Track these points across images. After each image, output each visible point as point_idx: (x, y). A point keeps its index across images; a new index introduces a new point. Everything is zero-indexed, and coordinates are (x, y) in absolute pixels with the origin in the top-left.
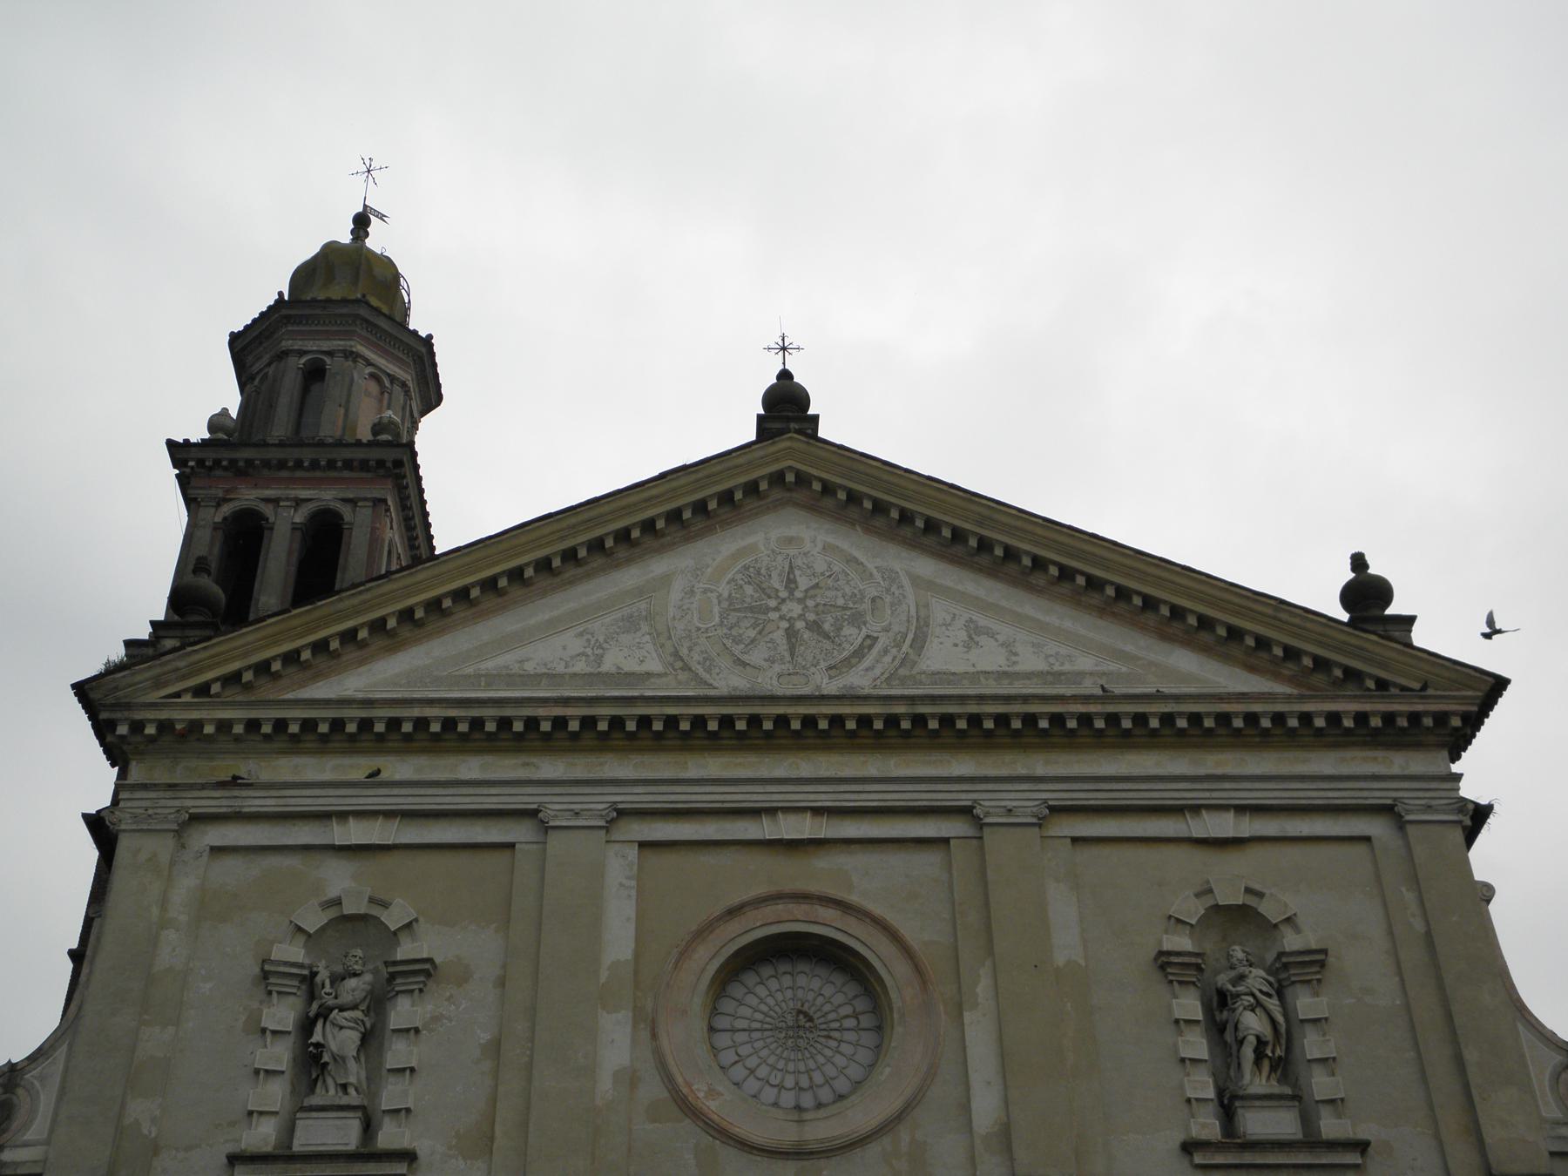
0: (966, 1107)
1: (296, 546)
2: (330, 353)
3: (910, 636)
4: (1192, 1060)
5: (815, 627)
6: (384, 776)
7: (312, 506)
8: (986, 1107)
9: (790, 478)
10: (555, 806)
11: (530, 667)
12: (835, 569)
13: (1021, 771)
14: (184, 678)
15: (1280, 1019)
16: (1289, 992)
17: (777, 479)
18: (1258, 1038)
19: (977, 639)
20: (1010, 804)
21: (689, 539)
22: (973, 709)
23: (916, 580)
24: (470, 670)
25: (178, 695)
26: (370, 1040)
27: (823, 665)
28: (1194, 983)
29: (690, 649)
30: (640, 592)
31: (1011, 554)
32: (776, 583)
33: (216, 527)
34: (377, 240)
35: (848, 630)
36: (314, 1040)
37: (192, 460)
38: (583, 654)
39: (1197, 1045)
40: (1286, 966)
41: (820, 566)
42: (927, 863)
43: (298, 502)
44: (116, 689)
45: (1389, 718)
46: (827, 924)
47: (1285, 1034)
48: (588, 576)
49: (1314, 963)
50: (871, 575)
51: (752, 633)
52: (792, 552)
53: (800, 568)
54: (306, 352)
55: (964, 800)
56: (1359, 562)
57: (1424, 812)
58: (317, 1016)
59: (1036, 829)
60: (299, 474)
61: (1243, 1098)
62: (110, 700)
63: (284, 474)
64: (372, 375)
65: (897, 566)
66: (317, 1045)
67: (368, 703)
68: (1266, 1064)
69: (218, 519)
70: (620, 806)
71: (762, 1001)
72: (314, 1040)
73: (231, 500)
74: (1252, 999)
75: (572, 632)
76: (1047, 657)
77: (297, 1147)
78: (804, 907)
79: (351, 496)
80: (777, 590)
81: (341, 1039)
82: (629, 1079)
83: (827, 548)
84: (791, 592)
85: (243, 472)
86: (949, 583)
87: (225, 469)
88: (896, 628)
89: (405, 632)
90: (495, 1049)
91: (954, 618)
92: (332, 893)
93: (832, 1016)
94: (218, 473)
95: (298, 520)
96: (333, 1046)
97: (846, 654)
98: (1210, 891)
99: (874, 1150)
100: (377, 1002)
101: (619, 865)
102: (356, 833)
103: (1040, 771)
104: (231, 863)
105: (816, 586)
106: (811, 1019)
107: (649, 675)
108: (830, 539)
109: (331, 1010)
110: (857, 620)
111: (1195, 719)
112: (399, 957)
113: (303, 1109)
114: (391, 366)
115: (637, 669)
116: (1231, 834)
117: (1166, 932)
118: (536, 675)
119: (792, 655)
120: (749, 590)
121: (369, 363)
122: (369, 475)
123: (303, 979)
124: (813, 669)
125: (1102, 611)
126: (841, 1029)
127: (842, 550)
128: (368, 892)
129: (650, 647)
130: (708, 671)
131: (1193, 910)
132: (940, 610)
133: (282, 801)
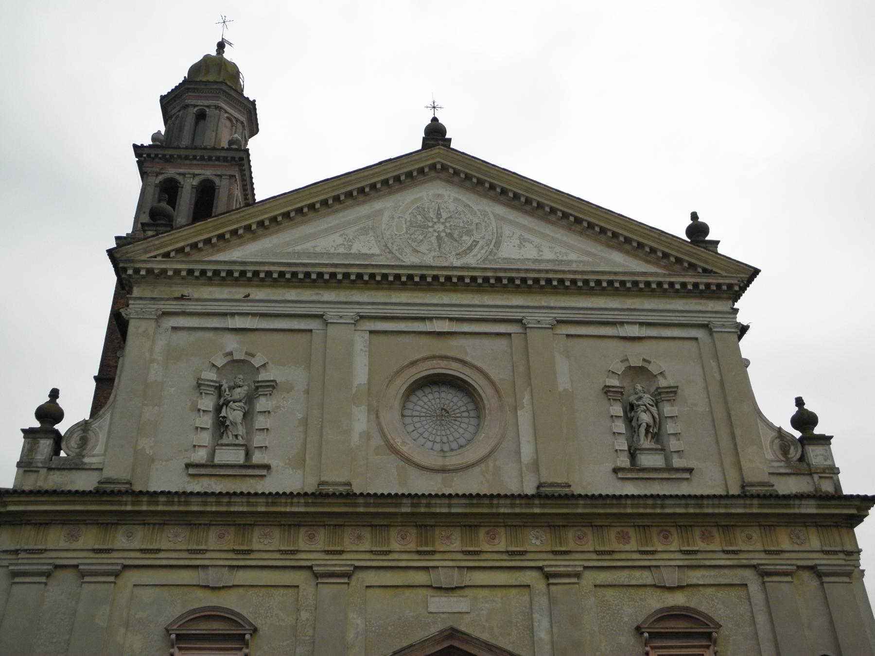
0: (518, 452)
1: (194, 195)
2: (208, 107)
3: (494, 241)
5: (450, 235)
6: (251, 297)
7: (201, 177)
8: (527, 452)
9: (439, 167)
10: (331, 313)
11: (318, 250)
14: (157, 249)
15: (657, 416)
16: (660, 405)
17: (433, 167)
19: (524, 244)
21: (391, 193)
22: (523, 275)
23: (496, 216)
24: (290, 250)
25: (155, 257)
26: (247, 415)
27: (454, 253)
30: (369, 216)
35: (465, 238)
37: (145, 154)
39: (620, 427)
40: (660, 393)
41: (452, 208)
42: (501, 344)
44: (127, 253)
45: (708, 286)
46: (455, 370)
48: (345, 209)
49: (673, 391)
51: (421, 237)
52: (439, 201)
54: (197, 106)
55: (518, 316)
61: (640, 450)
62: (124, 258)
63: (188, 162)
64: (228, 118)
65: (488, 209)
66: (224, 417)
68: (650, 435)
69: (157, 182)
71: (423, 408)
73: (163, 173)
75: (337, 234)
76: (556, 253)
77: (216, 461)
78: (445, 362)
79: (219, 173)
80: (432, 218)
81: (234, 414)
82: (366, 436)
83: (455, 200)
85: (168, 160)
87: (160, 159)
92: (228, 350)
93: (458, 411)
95: (194, 183)
98: (627, 360)
99: (477, 469)
100: (250, 399)
101: (360, 341)
104: (181, 334)
105: (450, 217)
106: (448, 412)
108: (457, 196)
110: (469, 233)
114: (236, 114)
115: (368, 252)
117: (608, 377)
118: (321, 253)
119: (440, 248)
120: (419, 218)
121: (226, 112)
123: (216, 387)
128: (245, 349)
131: (620, 368)
133: (204, 307)
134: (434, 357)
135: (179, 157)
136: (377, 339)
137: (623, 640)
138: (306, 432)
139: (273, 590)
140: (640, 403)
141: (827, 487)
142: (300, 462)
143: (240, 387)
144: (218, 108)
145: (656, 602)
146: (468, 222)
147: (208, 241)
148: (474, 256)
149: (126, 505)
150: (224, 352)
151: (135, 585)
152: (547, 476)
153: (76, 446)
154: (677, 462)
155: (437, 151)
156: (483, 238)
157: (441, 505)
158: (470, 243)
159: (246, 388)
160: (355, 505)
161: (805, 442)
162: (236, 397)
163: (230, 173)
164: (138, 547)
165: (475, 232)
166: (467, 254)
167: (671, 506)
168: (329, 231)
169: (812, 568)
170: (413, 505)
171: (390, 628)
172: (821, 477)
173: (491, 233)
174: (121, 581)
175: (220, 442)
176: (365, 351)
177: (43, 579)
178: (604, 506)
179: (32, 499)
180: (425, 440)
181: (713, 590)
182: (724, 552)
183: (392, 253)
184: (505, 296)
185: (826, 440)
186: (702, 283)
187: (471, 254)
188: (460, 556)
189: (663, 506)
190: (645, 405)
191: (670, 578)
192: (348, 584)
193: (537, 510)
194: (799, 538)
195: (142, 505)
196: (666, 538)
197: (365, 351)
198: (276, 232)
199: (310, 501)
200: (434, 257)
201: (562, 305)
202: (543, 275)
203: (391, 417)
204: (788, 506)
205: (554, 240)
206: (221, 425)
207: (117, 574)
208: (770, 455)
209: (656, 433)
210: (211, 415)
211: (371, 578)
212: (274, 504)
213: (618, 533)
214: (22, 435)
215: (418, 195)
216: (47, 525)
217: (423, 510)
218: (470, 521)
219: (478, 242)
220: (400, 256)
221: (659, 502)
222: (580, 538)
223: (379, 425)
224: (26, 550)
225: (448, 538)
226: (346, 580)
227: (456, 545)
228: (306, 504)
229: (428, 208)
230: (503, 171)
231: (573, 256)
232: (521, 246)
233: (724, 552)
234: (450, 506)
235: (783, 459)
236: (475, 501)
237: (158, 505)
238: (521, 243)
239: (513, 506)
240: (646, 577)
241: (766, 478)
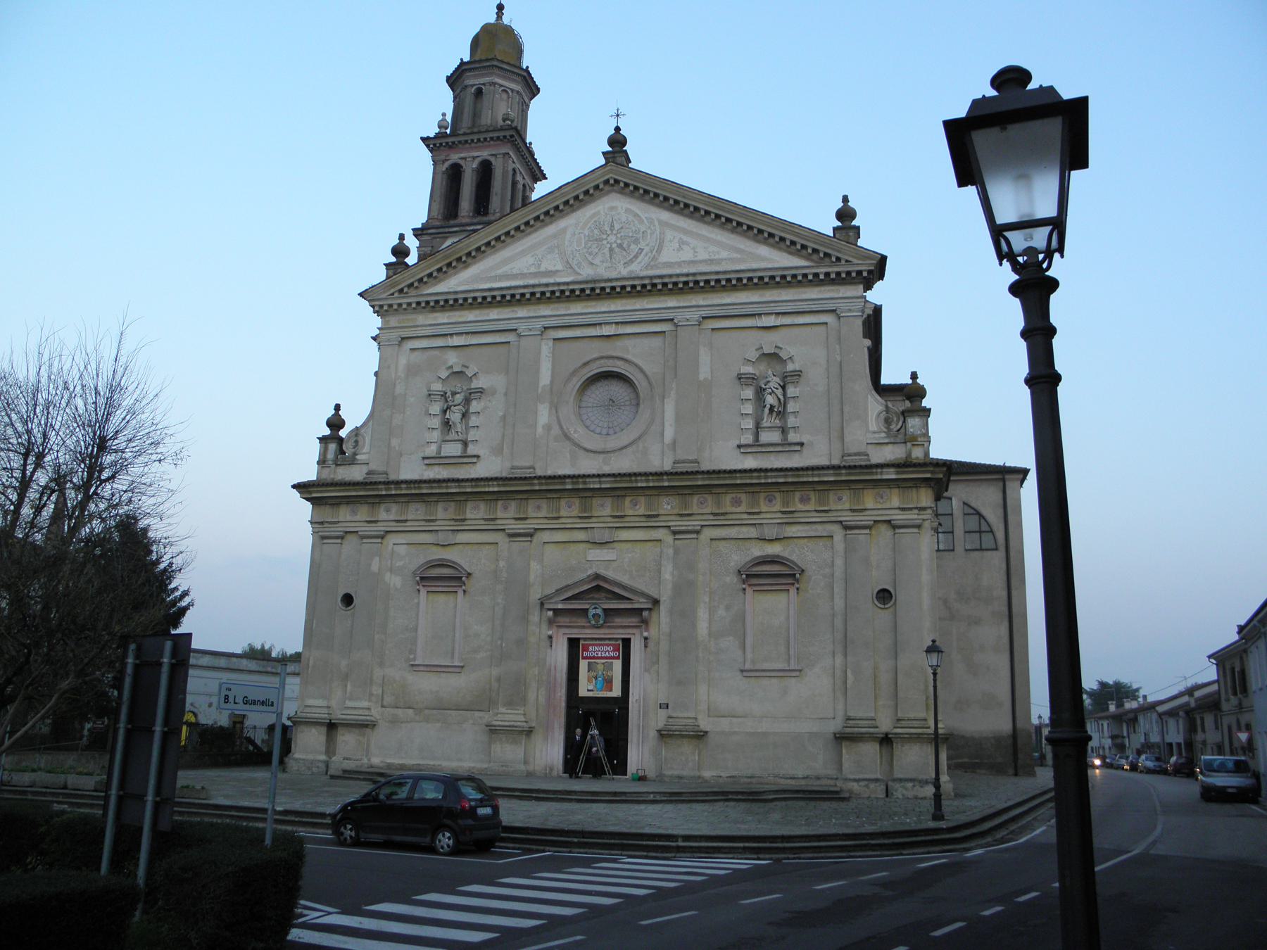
0: (662, 435)
1: (474, 178)
2: (484, 84)
3: (656, 247)
4: (745, 414)
5: (620, 246)
7: (480, 159)
8: (669, 434)
9: (612, 182)
10: (522, 327)
11: (514, 272)
12: (630, 219)
13: (694, 303)
17: (607, 182)
18: (771, 405)
19: (682, 246)
20: (688, 317)
21: (573, 211)
22: (674, 280)
23: (660, 222)
24: (493, 274)
25: (393, 294)
26: (465, 415)
27: (622, 262)
28: (751, 385)
29: (573, 259)
30: (555, 236)
31: (697, 209)
32: (607, 228)
33: (444, 173)
34: (506, 20)
35: (633, 246)
36: (446, 417)
38: (533, 264)
39: (749, 408)
40: (786, 377)
41: (624, 219)
42: (656, 342)
43: (474, 158)
45: (838, 274)
46: (620, 367)
48: (536, 230)
49: (798, 374)
50: (643, 221)
51: (597, 250)
52: (613, 213)
53: (615, 220)
54: (474, 85)
55: (671, 316)
56: (845, 199)
57: (848, 312)
58: (447, 409)
59: (697, 327)
63: (467, 145)
64: (503, 90)
65: (653, 216)
66: (448, 419)
67: (456, 293)
68: (775, 414)
69: (444, 169)
70: (546, 326)
71: (595, 400)
72: (446, 417)
74: (770, 390)
75: (530, 255)
77: (442, 454)
78: (611, 361)
79: (494, 153)
80: (606, 231)
81: (455, 416)
82: (548, 428)
83: (628, 211)
84: (612, 230)
85: (451, 146)
87: (444, 146)
88: (651, 245)
89: (469, 260)
90: (504, 418)
91: (674, 237)
92: (450, 364)
93: (622, 401)
95: (474, 166)
96: (452, 419)
97: (631, 257)
98: (762, 348)
99: (630, 450)
100: (467, 401)
101: (546, 348)
102: (457, 341)
103: (702, 303)
104: (416, 353)
105: (622, 228)
106: (614, 402)
107: (557, 271)
108: (629, 206)
109: (451, 406)
110: (636, 241)
111: (761, 278)
112: (472, 387)
113: (443, 441)
115: (554, 269)
116: (772, 324)
117: (743, 365)
118: (517, 274)
119: (611, 259)
121: (501, 86)
123: (442, 395)
124: (619, 265)
126: (625, 405)
127: (633, 211)
129: (558, 259)
130: (579, 268)
131: (753, 355)
132: (669, 234)
134: (602, 358)
135: (460, 142)
136: (559, 345)
137: (728, 579)
138: (504, 427)
139: (482, 546)
140: (767, 386)
141: (917, 453)
142: (498, 451)
143: (459, 393)
144: (494, 84)
145: (758, 551)
146: (636, 230)
147: (430, 275)
149: (382, 490)
150: (447, 366)
151: (394, 544)
152: (681, 455)
153: (352, 447)
154: (792, 437)
155: (609, 168)
156: (648, 245)
157: (594, 483)
159: (463, 394)
160: (533, 484)
161: (906, 414)
162: (456, 403)
163: (504, 152)
164: (393, 519)
165: (641, 241)
166: (632, 262)
167: (771, 477)
168: (523, 253)
169: (889, 522)
170: (573, 483)
171: (559, 572)
172: (913, 445)
173: (654, 240)
174: (385, 541)
175: (447, 438)
176: (549, 357)
177: (339, 541)
178: (719, 479)
179: (324, 489)
180: (595, 426)
181: (806, 540)
182: (816, 511)
183: (572, 268)
184: (662, 298)
185: (927, 412)
186: (832, 272)
188: (610, 519)
189: (766, 477)
190: (771, 388)
191: (770, 532)
192: (531, 541)
193: (666, 484)
194: (882, 498)
195: (391, 490)
196: (770, 501)
197: (549, 357)
198: (481, 260)
199: (501, 483)
200: (606, 268)
201: (709, 302)
202: (691, 278)
203: (568, 410)
204: (872, 474)
205: (708, 240)
206: (447, 424)
207: (382, 537)
208: (873, 426)
209: (780, 412)
210: (439, 417)
211: (546, 536)
212: (476, 486)
213: (733, 498)
214: (318, 441)
215: (597, 210)
216: (338, 504)
217: (581, 486)
218: (619, 493)
219: (643, 249)
220: (578, 270)
221: (762, 474)
222: (701, 503)
223: (558, 418)
224: (327, 522)
225: (602, 505)
226: (529, 539)
227: (607, 511)
228: (499, 486)
229: (603, 222)
230: (664, 181)
231: (724, 254)
232: (680, 249)
233: (816, 511)
234: (600, 482)
235: (885, 430)
236: (618, 479)
237: (402, 490)
238: (680, 247)
239: (647, 481)
240: (752, 532)
241: (863, 449)
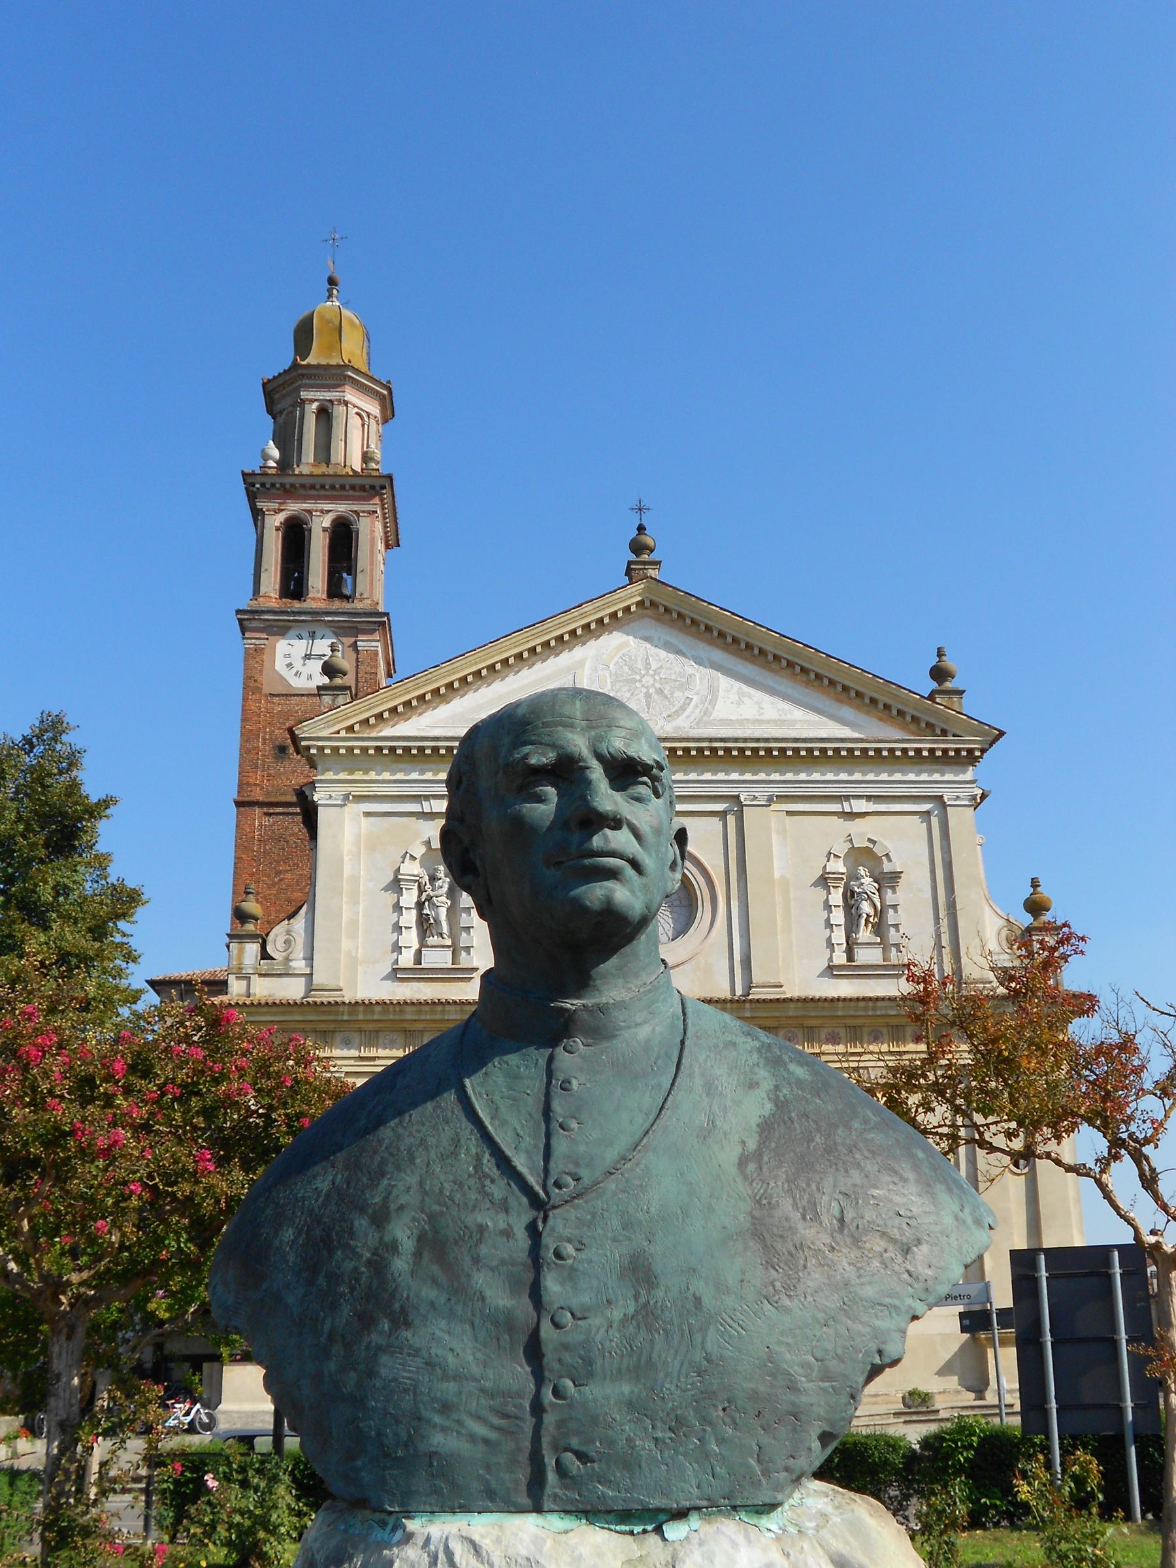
5: (660, 692)
15: (878, 905)
16: (883, 890)
25: (338, 732)
35: (677, 694)
47: (881, 914)
49: (895, 876)
60: (322, 493)
61: (858, 944)
63: (313, 492)
64: (357, 414)
73: (283, 510)
76: (779, 710)
86: (729, 666)
94: (274, 491)
105: (661, 667)
108: (668, 638)
114: (368, 406)
120: (626, 669)
122: (364, 494)
125: (808, 683)
148: (687, 717)
158: (682, 701)
187: (684, 716)
232: (740, 702)
